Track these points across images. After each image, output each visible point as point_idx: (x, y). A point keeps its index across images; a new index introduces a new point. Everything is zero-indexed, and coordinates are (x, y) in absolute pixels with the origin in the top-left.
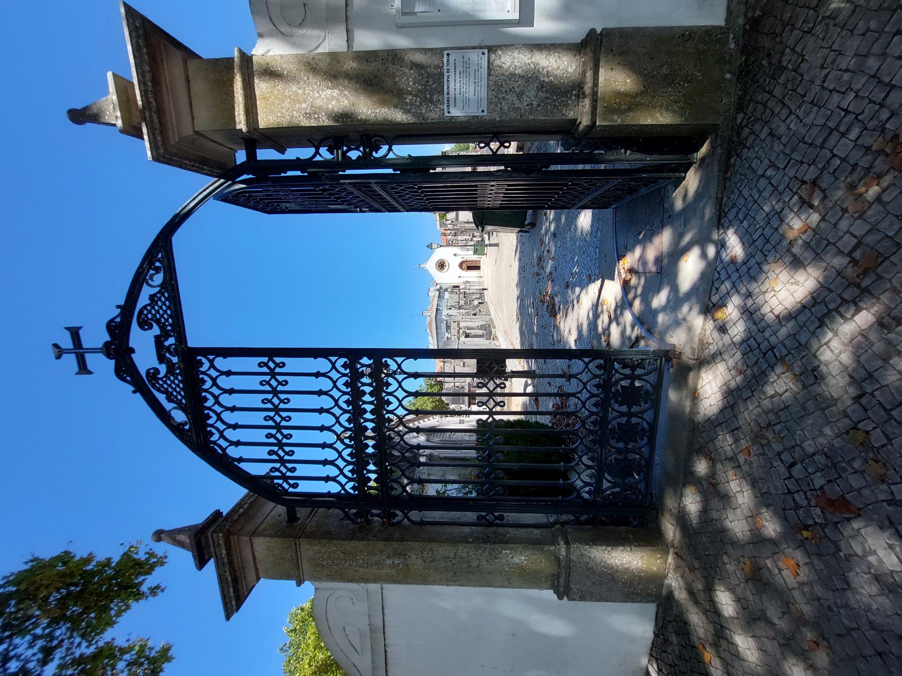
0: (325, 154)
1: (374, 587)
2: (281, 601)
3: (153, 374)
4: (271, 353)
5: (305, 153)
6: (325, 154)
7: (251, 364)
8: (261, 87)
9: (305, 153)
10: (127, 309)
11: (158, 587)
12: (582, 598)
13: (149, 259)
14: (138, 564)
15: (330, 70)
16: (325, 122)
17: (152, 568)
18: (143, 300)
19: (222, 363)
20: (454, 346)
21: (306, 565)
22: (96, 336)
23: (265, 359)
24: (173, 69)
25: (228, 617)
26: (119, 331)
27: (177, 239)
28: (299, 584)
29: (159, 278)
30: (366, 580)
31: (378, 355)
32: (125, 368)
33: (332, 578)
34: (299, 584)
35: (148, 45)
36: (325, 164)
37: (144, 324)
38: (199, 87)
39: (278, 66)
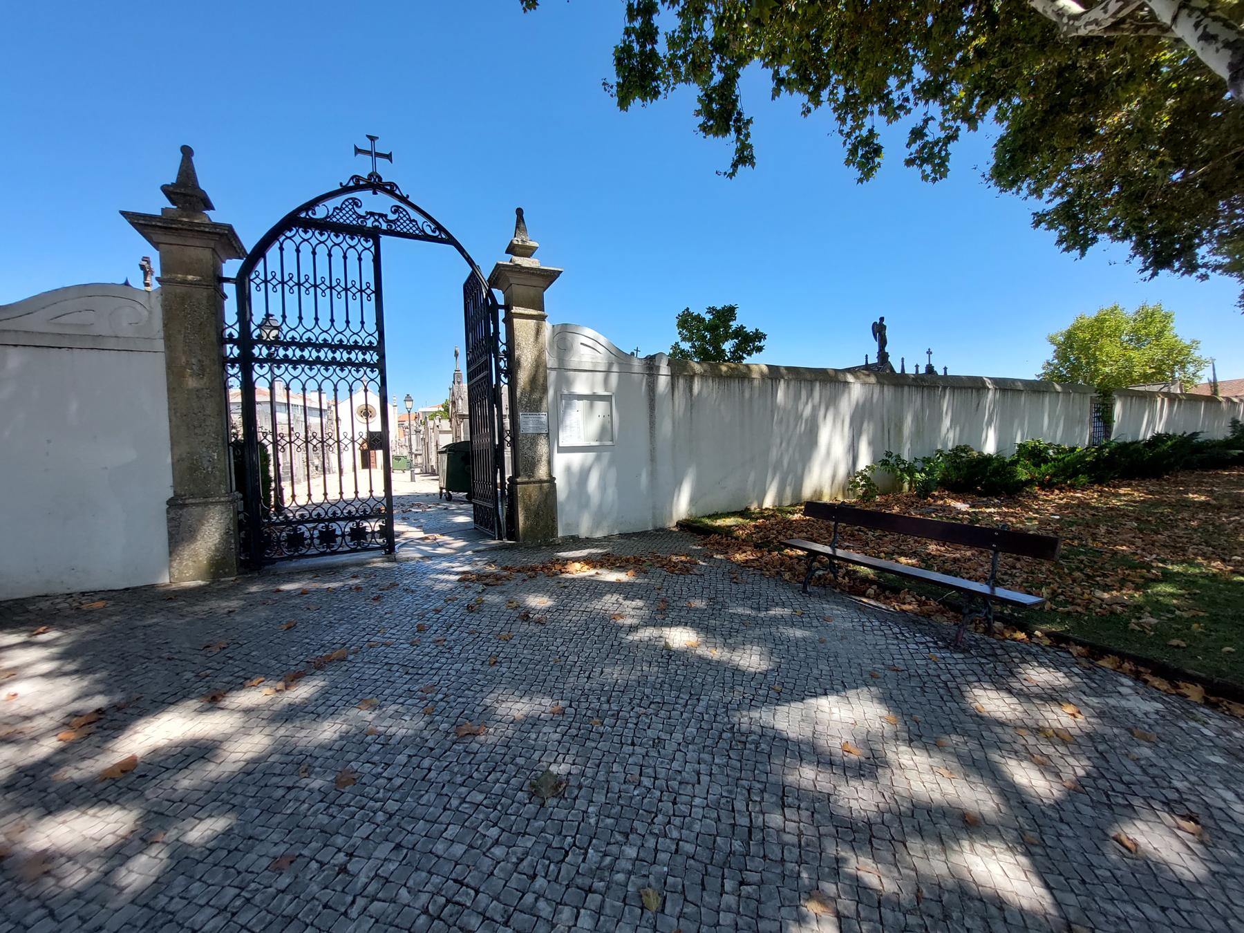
0: (503, 348)
1: (160, 345)
2: (128, 261)
4: (378, 292)
5: (503, 337)
6: (503, 348)
7: (369, 277)
8: (532, 323)
9: (503, 337)
10: (404, 199)
12: (170, 520)
13: (439, 227)
15: (539, 364)
16: (516, 354)
18: (414, 215)
19: (368, 257)
20: (390, 406)
22: (387, 172)
23: (373, 287)
28: (167, 190)
29: (429, 231)
30: (168, 338)
31: (380, 366)
32: (359, 184)
34: (167, 190)
35: (547, 276)
36: (497, 348)
37: (396, 210)
38: (532, 291)
39: (540, 340)
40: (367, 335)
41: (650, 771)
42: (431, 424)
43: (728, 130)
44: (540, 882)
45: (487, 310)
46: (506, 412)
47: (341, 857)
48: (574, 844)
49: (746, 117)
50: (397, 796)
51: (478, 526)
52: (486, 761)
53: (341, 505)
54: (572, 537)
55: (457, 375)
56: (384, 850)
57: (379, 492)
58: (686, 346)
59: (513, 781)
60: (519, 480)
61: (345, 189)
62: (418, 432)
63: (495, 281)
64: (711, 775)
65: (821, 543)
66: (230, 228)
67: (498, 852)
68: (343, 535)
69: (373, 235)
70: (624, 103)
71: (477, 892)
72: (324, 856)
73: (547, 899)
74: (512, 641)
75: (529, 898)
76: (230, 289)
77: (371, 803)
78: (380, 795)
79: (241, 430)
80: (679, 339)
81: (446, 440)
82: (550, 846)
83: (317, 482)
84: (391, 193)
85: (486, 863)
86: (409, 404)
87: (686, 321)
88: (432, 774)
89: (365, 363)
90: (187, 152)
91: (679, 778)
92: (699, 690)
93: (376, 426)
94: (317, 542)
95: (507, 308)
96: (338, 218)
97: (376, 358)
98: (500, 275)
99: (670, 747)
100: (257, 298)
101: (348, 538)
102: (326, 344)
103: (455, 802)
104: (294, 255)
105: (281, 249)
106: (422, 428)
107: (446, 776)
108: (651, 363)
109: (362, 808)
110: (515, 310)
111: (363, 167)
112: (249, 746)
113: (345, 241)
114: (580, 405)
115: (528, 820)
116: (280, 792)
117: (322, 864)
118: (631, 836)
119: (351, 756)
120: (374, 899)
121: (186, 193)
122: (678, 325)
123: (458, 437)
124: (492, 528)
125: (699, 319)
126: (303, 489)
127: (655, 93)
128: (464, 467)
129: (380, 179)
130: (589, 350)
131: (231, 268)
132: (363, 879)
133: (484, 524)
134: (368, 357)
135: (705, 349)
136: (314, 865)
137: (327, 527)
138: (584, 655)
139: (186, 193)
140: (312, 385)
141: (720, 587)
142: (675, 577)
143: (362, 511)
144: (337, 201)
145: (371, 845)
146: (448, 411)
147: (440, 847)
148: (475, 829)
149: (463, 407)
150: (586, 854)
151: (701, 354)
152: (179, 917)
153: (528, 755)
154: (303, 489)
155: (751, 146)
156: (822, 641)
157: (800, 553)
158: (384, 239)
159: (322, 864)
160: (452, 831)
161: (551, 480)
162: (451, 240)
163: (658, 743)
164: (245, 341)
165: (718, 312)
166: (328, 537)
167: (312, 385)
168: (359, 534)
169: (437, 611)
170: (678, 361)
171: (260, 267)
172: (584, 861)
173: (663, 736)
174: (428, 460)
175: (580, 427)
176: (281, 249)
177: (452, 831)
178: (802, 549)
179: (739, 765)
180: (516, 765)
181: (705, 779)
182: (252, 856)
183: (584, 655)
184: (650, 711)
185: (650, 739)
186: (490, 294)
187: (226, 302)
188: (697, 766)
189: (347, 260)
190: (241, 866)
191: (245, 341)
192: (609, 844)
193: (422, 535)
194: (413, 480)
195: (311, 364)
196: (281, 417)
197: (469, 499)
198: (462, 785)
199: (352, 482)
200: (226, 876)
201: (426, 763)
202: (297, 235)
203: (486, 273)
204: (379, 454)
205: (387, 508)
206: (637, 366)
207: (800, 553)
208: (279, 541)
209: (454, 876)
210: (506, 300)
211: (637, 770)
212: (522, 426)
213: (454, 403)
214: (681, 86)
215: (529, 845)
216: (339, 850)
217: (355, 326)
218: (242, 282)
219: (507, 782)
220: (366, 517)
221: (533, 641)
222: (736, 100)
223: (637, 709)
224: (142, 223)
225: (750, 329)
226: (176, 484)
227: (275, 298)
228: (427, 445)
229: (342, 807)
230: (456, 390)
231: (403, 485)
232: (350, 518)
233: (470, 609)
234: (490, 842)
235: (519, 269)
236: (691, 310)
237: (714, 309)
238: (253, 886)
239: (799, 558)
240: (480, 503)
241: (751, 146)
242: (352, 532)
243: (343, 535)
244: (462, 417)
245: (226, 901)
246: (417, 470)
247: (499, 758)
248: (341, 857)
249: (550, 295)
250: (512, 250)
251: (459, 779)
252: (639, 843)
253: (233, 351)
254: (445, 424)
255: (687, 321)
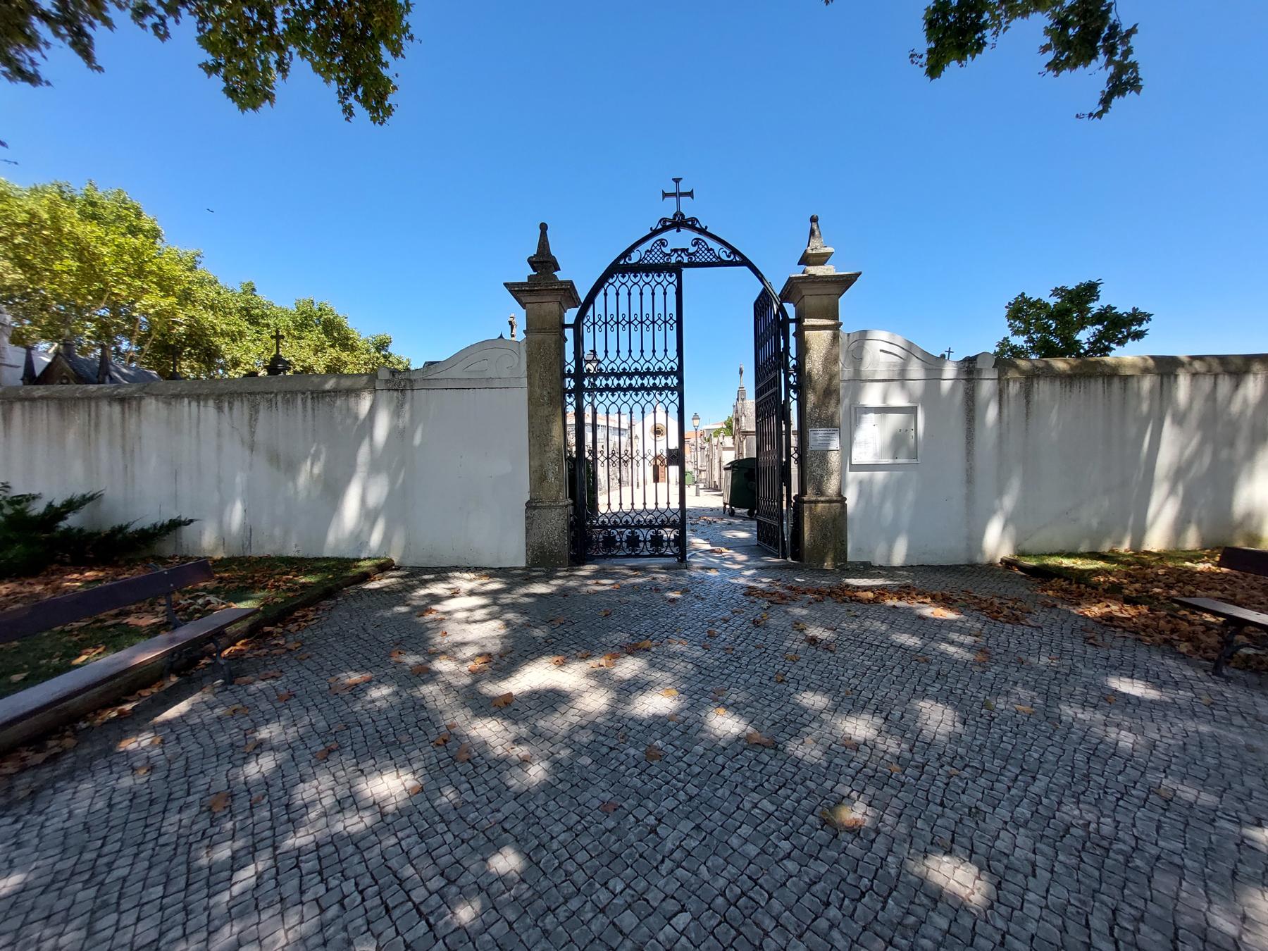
0: (792, 363)
1: (525, 382)
2: (507, 320)
3: (663, 243)
5: (793, 352)
6: (792, 363)
7: (672, 309)
8: (827, 334)
9: (793, 352)
10: (703, 231)
11: (351, 114)
12: (527, 518)
13: (735, 251)
14: (382, 97)
17: (373, 110)
18: (712, 244)
19: (672, 290)
21: (539, 337)
22: (689, 209)
24: (833, 289)
25: (506, 284)
26: (692, 224)
27: (746, 268)
29: (724, 257)
30: (529, 377)
31: (679, 389)
32: (666, 225)
33: (530, 354)
36: (787, 363)
37: (696, 242)
40: (670, 364)
41: (965, 841)
42: (715, 441)
43: (1093, 55)
44: (833, 912)
45: (773, 327)
46: (794, 427)
47: (651, 820)
48: (871, 888)
49: (1125, 28)
50: (696, 782)
51: (761, 543)
52: (776, 774)
53: (633, 515)
54: (864, 563)
55: (741, 395)
56: (686, 826)
57: (675, 505)
58: (1019, 341)
59: (804, 802)
60: (805, 498)
61: (655, 232)
62: (702, 448)
63: (786, 295)
64: (1052, 872)
65: (1254, 609)
66: (571, 283)
67: (791, 866)
68: (645, 541)
69: (676, 269)
70: (934, 70)
71: (770, 897)
72: (640, 813)
73: (841, 932)
74: (799, 663)
75: (822, 924)
76: (569, 333)
77: (674, 781)
78: (682, 776)
79: (574, 449)
80: (1008, 333)
81: (729, 457)
82: (844, 880)
83: (615, 495)
84: (693, 228)
85: (779, 874)
86: (696, 422)
87: (1020, 310)
88: (726, 772)
89: (666, 387)
90: (544, 227)
91: (1005, 861)
92: (1034, 767)
93: (674, 444)
94: (625, 545)
95: (799, 321)
96: (650, 260)
97: (676, 381)
98: (792, 289)
99: (993, 824)
100: (588, 337)
101: (648, 544)
102: (637, 372)
103: (747, 805)
104: (623, 298)
105: (606, 294)
106: (706, 445)
107: (738, 778)
108: (970, 367)
109: (667, 783)
110: (807, 322)
111: (668, 209)
112: (596, 702)
113: (652, 279)
114: (871, 418)
115: (821, 846)
116: (605, 750)
117: (638, 820)
118: (939, 904)
119: (656, 734)
120: (679, 866)
121: (543, 262)
122: (1008, 317)
123: (740, 453)
124: (776, 546)
125: (1039, 305)
126: (616, 498)
127: (980, 46)
128: (749, 484)
129: (682, 215)
130: (881, 353)
131: (570, 315)
132: (669, 845)
133: (767, 540)
134: (669, 381)
135: (1047, 342)
136: (631, 818)
137: (633, 533)
138: (880, 694)
139: (543, 262)
140: (613, 409)
141: (1068, 646)
142: (998, 624)
143: (658, 521)
144: (647, 245)
145: (675, 818)
146: (731, 428)
147: (734, 841)
148: (768, 836)
149: (749, 423)
150: (885, 903)
151: (1041, 348)
152: (543, 822)
153: (819, 782)
154: (616, 498)
155: (1134, 66)
156: (1250, 749)
157: (1209, 618)
158: (685, 271)
159: (638, 820)
160: (745, 830)
161: (842, 500)
162: (745, 262)
163: (974, 812)
164: (579, 375)
165: (1070, 292)
166: (633, 542)
167: (613, 409)
168: (657, 541)
169: (726, 621)
170: (1005, 358)
171: (590, 313)
172: (883, 909)
173: (983, 807)
174: (712, 476)
175: (871, 440)
176: (606, 294)
177: (745, 830)
178: (1215, 614)
179: (1097, 873)
180: (807, 787)
181: (1043, 875)
182: (588, 795)
183: (880, 694)
184: (965, 774)
185: (965, 806)
186: (781, 309)
187: (566, 344)
188: (1031, 855)
189: (652, 296)
190: (580, 799)
191: (579, 375)
192: (912, 903)
193: (708, 547)
194: (697, 494)
195: (636, 390)
196: (601, 434)
197: (751, 516)
198: (753, 790)
199: (658, 496)
200: (571, 804)
201: (720, 760)
202: (617, 280)
203: (777, 289)
204: (674, 471)
205: (682, 520)
206: (950, 371)
207: (1209, 618)
208: (598, 542)
209: (748, 872)
210: (797, 313)
211: (948, 835)
212: (811, 442)
213: (737, 420)
214: (1017, 23)
215: (823, 871)
216: (650, 813)
217: (660, 354)
218: (577, 327)
219: (799, 802)
220: (663, 526)
221: (821, 667)
222: (1109, 11)
223: (947, 767)
224: (516, 290)
225: (1123, 308)
226: (531, 491)
227: (600, 336)
228: (710, 461)
229: (651, 777)
230: (740, 407)
231: (699, 499)
232: (650, 526)
233: (756, 623)
234: (781, 855)
235: (814, 279)
236: (1027, 295)
237: (1063, 289)
238: (589, 818)
239: (1208, 627)
240: (765, 520)
241: (1134, 66)
242: (664, 537)
243: (645, 541)
244: (746, 433)
245: (572, 823)
246: (701, 486)
247: (789, 775)
248: (651, 820)
249: (846, 302)
250: (806, 260)
251: (751, 784)
252: (951, 916)
253: (570, 383)
254: (728, 441)
255: (1021, 311)
